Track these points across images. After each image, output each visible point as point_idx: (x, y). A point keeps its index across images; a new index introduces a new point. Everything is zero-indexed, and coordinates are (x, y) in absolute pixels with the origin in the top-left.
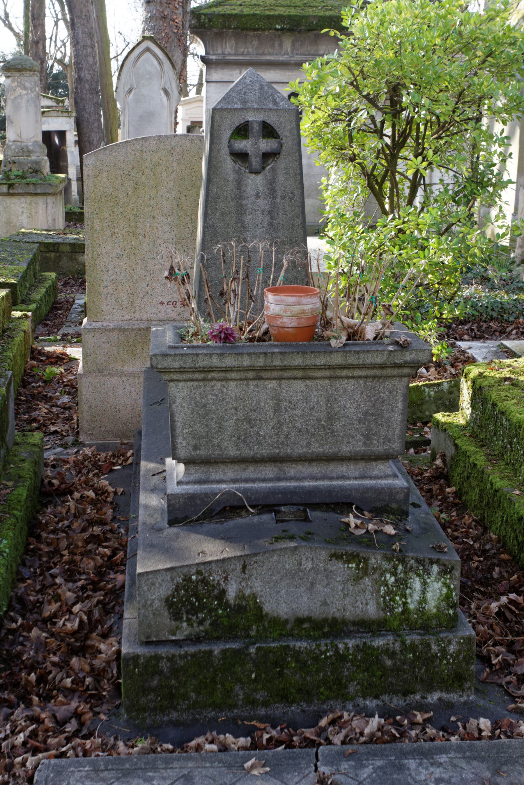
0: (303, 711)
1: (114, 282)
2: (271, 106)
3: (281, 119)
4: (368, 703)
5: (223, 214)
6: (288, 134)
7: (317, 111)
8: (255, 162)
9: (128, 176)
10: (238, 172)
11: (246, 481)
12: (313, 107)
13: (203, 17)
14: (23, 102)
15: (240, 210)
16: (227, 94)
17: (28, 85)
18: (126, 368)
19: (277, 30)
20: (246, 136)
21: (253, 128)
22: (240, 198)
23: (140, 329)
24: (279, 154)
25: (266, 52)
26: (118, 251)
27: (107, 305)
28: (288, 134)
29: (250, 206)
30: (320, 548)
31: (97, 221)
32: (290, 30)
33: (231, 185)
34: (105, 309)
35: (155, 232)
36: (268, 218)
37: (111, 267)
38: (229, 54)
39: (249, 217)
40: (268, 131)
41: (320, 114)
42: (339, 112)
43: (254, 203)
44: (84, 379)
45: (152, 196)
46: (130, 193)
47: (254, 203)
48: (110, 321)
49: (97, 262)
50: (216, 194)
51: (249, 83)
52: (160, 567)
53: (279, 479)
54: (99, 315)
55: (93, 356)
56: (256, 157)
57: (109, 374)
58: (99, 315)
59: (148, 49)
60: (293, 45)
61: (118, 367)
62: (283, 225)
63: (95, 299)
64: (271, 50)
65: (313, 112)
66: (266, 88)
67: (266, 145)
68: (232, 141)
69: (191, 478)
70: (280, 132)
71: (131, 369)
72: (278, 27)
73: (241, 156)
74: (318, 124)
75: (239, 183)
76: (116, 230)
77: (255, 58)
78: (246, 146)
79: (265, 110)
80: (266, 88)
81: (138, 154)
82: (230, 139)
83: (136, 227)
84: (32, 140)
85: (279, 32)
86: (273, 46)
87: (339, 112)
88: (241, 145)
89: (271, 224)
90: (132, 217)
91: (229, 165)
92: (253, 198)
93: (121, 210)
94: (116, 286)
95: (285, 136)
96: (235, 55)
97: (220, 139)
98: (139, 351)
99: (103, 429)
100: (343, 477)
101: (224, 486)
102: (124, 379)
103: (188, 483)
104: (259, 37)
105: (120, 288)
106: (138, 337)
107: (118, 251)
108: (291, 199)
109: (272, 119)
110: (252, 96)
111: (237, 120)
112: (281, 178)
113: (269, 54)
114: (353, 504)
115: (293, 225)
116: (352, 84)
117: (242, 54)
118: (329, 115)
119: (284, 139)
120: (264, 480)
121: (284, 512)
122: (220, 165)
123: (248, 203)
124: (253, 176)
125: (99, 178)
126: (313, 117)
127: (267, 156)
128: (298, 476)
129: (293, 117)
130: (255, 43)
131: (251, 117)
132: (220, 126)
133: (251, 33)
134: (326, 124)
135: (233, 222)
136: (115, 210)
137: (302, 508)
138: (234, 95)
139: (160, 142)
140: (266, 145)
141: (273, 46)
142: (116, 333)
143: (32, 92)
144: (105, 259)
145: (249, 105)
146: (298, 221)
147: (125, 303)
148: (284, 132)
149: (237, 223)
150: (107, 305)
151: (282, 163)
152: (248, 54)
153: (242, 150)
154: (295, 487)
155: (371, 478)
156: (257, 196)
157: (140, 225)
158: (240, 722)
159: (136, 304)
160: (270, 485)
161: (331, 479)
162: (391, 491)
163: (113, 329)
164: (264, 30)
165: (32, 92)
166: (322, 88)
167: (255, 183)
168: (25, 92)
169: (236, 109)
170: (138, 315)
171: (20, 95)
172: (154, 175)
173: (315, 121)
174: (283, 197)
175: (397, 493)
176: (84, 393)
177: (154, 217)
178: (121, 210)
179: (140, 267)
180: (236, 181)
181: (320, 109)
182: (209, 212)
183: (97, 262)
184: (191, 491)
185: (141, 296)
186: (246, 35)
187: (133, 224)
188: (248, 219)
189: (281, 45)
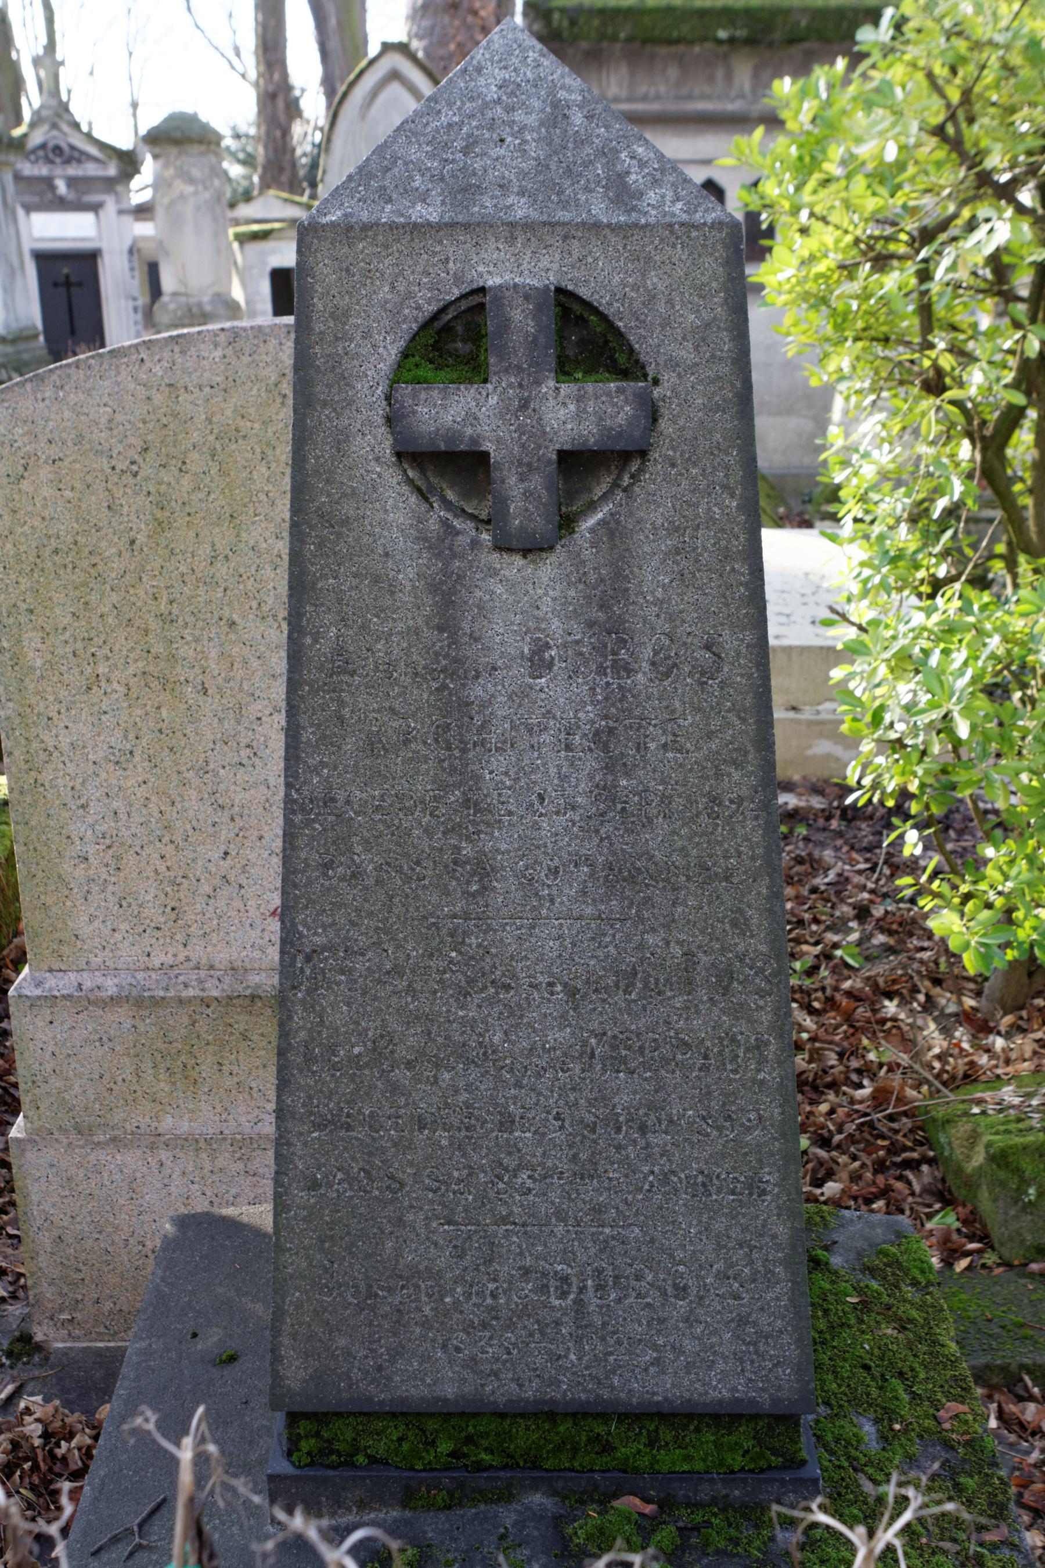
1: (109, 843)
2: (599, 209)
3: (653, 279)
5: (373, 746)
6: (686, 354)
7: (817, 226)
8: (523, 496)
9: (128, 479)
10: (440, 545)
12: (804, 214)
13: (556, 16)
14: (189, 208)
15: (457, 726)
16: (380, 150)
17: (196, 173)
18: (167, 1123)
19: (719, 42)
20: (474, 371)
21: (505, 324)
22: (452, 668)
23: (205, 1002)
24: (643, 454)
25: (697, 92)
26: (116, 739)
27: (92, 918)
28: (686, 354)
29: (501, 708)
31: (31, 640)
32: (751, 42)
33: (411, 607)
34: (86, 931)
35: (239, 673)
36: (590, 763)
37: (93, 792)
38: (617, 100)
39: (499, 762)
40: (586, 338)
41: (826, 236)
42: (889, 231)
43: (524, 693)
44: (31, 1155)
45: (222, 546)
46: (141, 539)
47: (524, 693)
48: (105, 970)
49: (46, 777)
50: (340, 650)
51: (493, 92)
54: (65, 949)
55: (56, 1083)
56: (526, 470)
57: (114, 1139)
58: (65, 949)
59: (395, 75)
60: (756, 74)
61: (141, 1118)
62: (665, 799)
63: (49, 901)
64: (707, 89)
65: (804, 231)
66: (578, 118)
67: (572, 411)
68: (405, 391)
70: (647, 343)
71: (185, 1127)
72: (722, 34)
73: (452, 468)
74: (821, 267)
75: (447, 597)
76: (102, 669)
77: (672, 107)
78: (472, 418)
79: (567, 232)
80: (578, 118)
81: (158, 398)
82: (395, 381)
83: (172, 658)
84: (211, 291)
85: (725, 48)
86: (711, 79)
87: (889, 231)
88: (452, 410)
89: (606, 793)
90: (154, 624)
91: (393, 510)
92: (519, 671)
93: (114, 598)
94: (118, 858)
95: (673, 364)
96: (630, 99)
97: (344, 380)
98: (206, 1069)
99: (108, 1306)
102: (164, 1155)
104: (680, 59)
105: (130, 860)
106: (202, 1027)
107: (116, 739)
108: (704, 675)
109: (603, 280)
110: (502, 160)
111: (426, 287)
112: (652, 576)
113: (704, 97)
115: (715, 800)
116: (939, 131)
117: (645, 99)
118: (857, 241)
119: (668, 379)
122: (348, 509)
123: (493, 695)
124: (514, 566)
125: (25, 485)
126: (804, 246)
127: (578, 466)
129: (711, 268)
130: (673, 72)
131: (497, 269)
132: (340, 316)
133: (663, 51)
134: (848, 270)
135: (423, 786)
136: (93, 598)
138: (414, 153)
139: (239, 354)
140: (572, 411)
141: (711, 79)
142: (123, 1015)
143: (206, 188)
144: (71, 768)
145: (486, 205)
146: (738, 782)
147: (153, 913)
148: (669, 341)
149: (445, 787)
150: (92, 918)
151: (655, 501)
152: (657, 98)
153: (453, 436)
156: (538, 661)
157: (186, 651)
159: (190, 917)
163: (115, 1001)
164: (691, 42)
165: (206, 188)
166: (836, 152)
167: (525, 598)
168: (190, 189)
169: (417, 229)
170: (198, 951)
171: (182, 197)
172: (223, 473)
173: (812, 259)
174: (665, 668)
176: (35, 1198)
177: (232, 624)
178: (114, 598)
179: (193, 794)
180: (433, 588)
181: (824, 220)
182: (308, 735)
183: (46, 777)
185: (207, 889)
186: (652, 57)
187: (159, 648)
188: (495, 770)
189: (729, 77)
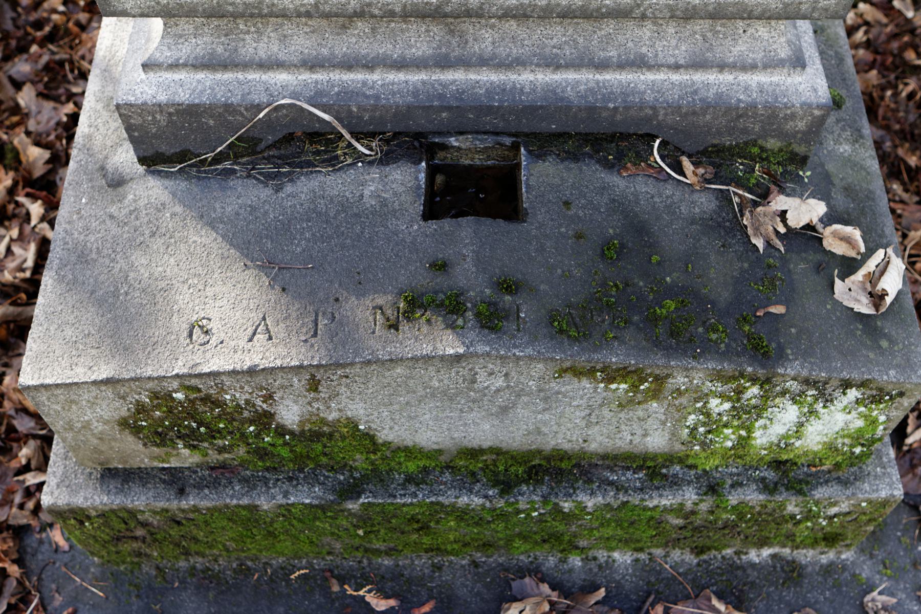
0: (475, 564)
4: (616, 555)
11: (348, 65)
30: (530, 358)
52: (81, 374)
53: (444, 63)
69: (185, 51)
100: (640, 63)
101: (282, 77)
103: (174, 66)
114: (653, 137)
120: (401, 65)
121: (459, 149)
128: (502, 51)
137: (508, 141)
154: (492, 90)
155: (722, 67)
158: (336, 588)
160: (416, 77)
161: (602, 66)
162: (773, 115)
175: (793, 116)
184: (183, 97)
